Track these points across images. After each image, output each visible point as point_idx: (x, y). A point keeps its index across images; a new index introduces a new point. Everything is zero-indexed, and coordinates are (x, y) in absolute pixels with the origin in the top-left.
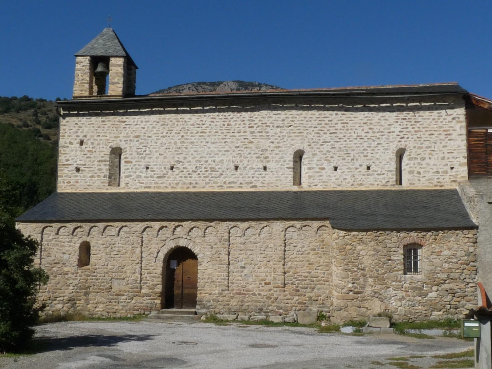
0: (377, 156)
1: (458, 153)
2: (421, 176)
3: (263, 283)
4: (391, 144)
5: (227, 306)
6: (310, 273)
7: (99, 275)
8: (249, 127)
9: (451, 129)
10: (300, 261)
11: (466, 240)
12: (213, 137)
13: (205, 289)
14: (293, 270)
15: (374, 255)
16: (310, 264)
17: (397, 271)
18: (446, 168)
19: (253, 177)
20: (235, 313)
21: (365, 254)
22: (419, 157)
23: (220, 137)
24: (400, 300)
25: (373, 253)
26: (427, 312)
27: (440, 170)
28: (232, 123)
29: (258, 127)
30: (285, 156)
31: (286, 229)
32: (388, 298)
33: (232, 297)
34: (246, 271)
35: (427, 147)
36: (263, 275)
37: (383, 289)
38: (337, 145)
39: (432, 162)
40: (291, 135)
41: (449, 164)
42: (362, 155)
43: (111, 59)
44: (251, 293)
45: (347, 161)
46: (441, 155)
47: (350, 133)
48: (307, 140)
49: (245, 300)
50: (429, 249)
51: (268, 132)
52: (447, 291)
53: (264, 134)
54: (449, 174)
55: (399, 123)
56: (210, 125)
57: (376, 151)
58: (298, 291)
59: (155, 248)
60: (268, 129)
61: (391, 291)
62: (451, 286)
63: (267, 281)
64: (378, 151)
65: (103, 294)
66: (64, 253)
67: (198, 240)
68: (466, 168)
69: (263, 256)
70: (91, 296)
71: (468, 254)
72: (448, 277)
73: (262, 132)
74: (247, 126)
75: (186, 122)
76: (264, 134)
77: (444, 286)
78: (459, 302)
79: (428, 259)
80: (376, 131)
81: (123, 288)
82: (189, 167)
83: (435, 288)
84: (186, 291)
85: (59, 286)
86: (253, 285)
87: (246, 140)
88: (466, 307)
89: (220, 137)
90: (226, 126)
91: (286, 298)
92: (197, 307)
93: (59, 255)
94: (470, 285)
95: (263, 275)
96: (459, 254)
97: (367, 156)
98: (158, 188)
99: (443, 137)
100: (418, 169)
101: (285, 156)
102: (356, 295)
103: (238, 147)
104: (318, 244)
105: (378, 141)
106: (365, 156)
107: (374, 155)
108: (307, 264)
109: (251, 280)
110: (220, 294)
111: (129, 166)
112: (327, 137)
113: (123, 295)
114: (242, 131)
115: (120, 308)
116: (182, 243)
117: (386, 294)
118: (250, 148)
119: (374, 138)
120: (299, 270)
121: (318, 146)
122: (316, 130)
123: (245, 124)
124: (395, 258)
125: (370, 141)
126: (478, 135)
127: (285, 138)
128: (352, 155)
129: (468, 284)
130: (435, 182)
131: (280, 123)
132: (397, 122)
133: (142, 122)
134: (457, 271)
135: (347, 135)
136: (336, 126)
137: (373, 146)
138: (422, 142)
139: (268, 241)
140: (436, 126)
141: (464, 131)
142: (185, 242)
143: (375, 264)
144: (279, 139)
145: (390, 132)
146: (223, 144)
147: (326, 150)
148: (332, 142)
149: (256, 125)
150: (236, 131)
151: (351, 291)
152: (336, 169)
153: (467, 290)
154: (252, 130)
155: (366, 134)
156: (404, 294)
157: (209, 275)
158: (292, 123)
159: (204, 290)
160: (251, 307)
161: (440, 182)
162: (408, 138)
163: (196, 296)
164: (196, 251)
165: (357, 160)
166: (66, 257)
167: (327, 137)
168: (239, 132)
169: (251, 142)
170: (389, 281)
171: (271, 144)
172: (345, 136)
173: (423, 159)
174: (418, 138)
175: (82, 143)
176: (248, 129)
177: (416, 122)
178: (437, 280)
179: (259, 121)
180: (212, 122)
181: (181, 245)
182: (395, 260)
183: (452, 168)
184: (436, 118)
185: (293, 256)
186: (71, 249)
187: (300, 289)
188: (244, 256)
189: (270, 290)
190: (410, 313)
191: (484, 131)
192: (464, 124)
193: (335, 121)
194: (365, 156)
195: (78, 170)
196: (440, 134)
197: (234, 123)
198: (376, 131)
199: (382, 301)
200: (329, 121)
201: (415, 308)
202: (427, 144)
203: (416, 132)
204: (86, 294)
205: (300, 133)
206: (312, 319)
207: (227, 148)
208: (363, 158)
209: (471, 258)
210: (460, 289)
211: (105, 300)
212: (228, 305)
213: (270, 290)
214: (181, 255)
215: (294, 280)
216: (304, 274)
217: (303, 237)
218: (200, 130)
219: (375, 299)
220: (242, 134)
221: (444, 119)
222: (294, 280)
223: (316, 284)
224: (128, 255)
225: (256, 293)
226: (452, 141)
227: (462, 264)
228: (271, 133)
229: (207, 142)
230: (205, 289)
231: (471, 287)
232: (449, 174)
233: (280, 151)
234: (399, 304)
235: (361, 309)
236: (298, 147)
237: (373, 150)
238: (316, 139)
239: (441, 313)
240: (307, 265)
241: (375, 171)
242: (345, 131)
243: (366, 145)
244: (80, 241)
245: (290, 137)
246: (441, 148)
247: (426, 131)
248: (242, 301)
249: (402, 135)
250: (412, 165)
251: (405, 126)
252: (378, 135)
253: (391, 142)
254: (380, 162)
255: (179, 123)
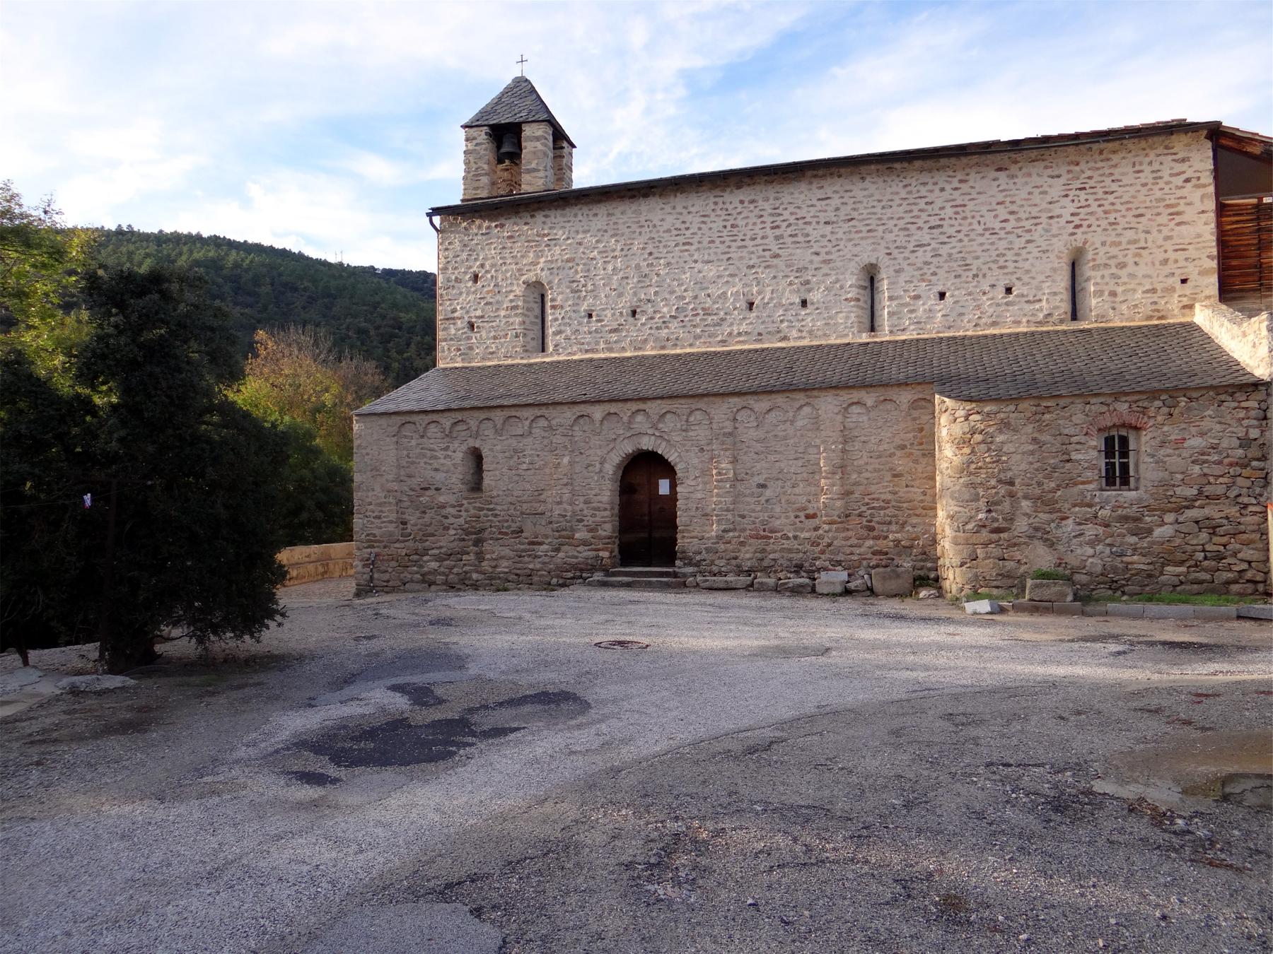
0: (1027, 265)
1: (1197, 249)
2: (1119, 299)
3: (802, 514)
4: (1055, 240)
5: (734, 562)
6: (895, 493)
7: (499, 507)
8: (772, 228)
9: (1182, 202)
10: (875, 470)
11: (1242, 414)
12: (706, 252)
13: (691, 528)
14: (861, 488)
15: (1032, 453)
16: (895, 476)
17: (1083, 483)
18: (1171, 281)
19: (782, 321)
20: (748, 573)
21: (1013, 450)
22: (1112, 262)
23: (719, 251)
24: (1092, 544)
25: (1031, 447)
26: (1151, 567)
27: (1159, 287)
28: (740, 222)
29: (789, 225)
30: (841, 277)
31: (846, 409)
32: (1065, 540)
33: (742, 544)
34: (768, 493)
35: (1129, 243)
36: (803, 499)
37: (1053, 521)
38: (944, 250)
39: (1141, 270)
40: (852, 236)
41: (1178, 272)
42: (994, 266)
43: (525, 127)
44: (779, 535)
45: (964, 279)
46: (1162, 256)
47: (970, 224)
48: (883, 244)
49: (768, 549)
50: (1155, 434)
51: (807, 235)
52: (1197, 522)
53: (800, 239)
54: (1179, 292)
55: (1070, 198)
56: (700, 229)
57: (1024, 256)
58: (872, 529)
59: (596, 455)
60: (809, 229)
61: (1069, 525)
62: (1207, 511)
63: (810, 512)
64: (1029, 256)
65: (506, 542)
66: (436, 470)
67: (676, 437)
68: (1214, 279)
69: (800, 463)
70: (487, 546)
71: (1245, 443)
72: (1200, 492)
73: (796, 235)
74: (768, 225)
75: (655, 226)
76: (800, 239)
77: (1191, 513)
78: (1225, 546)
79: (1153, 456)
80: (1023, 216)
81: (542, 530)
82: (665, 310)
83: (1170, 518)
84: (657, 535)
85: (430, 530)
86: (783, 520)
87: (767, 253)
88: (1240, 556)
89: (719, 251)
90: (729, 228)
91: (849, 543)
92: (678, 563)
93: (429, 473)
94: (1251, 508)
95: (803, 499)
96: (1225, 444)
97: (1005, 267)
98: (611, 350)
99: (1164, 219)
100: (1112, 287)
101: (841, 277)
102: (995, 536)
103: (753, 267)
104: (911, 435)
105: (1028, 237)
106: (1001, 268)
107: (1020, 265)
108: (888, 477)
109: (778, 510)
110: (719, 538)
111: (559, 314)
112: (925, 237)
113: (540, 544)
114: (759, 237)
115: (538, 566)
116: (647, 444)
117: (1060, 531)
118: (776, 266)
119: (1019, 231)
120: (873, 488)
121: (906, 255)
122: (901, 223)
123: (763, 222)
124: (1080, 457)
125: (1011, 237)
126: (1239, 210)
127: (842, 243)
128: (974, 267)
129: (1246, 506)
130: (1146, 309)
131: (830, 216)
132: (1067, 196)
133: (577, 232)
134: (1221, 480)
135: (965, 229)
136: (942, 212)
137: (1016, 246)
138: (1119, 231)
139: (810, 434)
140: (1148, 199)
141: (1211, 205)
142: (652, 443)
143: (1037, 470)
144: (830, 245)
145: (1051, 217)
146: (725, 263)
147: (921, 260)
148: (934, 245)
149: (785, 224)
150: (748, 237)
151: (984, 526)
152: (942, 295)
153: (1242, 520)
154: (777, 232)
155: (1004, 225)
156: (1101, 530)
157: (702, 503)
158: (855, 214)
159: (689, 531)
160: (779, 562)
161: (1158, 311)
162: (1089, 226)
163: (674, 541)
164: (672, 457)
165: (984, 276)
166: (440, 476)
167: (925, 237)
168: (754, 239)
169: (777, 256)
170: (1066, 506)
171: (815, 258)
172: (959, 231)
173: (1122, 266)
174: (1111, 224)
175: (476, 278)
176: (769, 232)
177: (1106, 193)
178: (1173, 500)
179: (792, 214)
180: (704, 222)
181: (645, 448)
182: (1077, 461)
183: (1184, 281)
184: (1150, 181)
185: (861, 462)
186: (448, 462)
187: (877, 526)
188: (763, 464)
189: (816, 529)
190: (1115, 570)
191: (1254, 201)
192: (1211, 189)
193: (939, 203)
194: (1001, 268)
195: (472, 326)
196: (1158, 214)
197: (744, 223)
198: (1023, 216)
199: (1052, 545)
200: (927, 203)
201: (1125, 559)
202: (1130, 234)
203: (1106, 212)
204: (478, 542)
205: (869, 231)
206: (905, 582)
207: (732, 269)
208: (997, 272)
209: (1254, 452)
210: (1227, 518)
211: (512, 554)
212: (735, 558)
213: (816, 529)
214: (644, 468)
215: (864, 508)
216: (883, 497)
217: (879, 424)
218: (681, 239)
219: (1036, 542)
220: (759, 241)
221: (1167, 183)
222: (864, 508)
223: (909, 516)
224: (547, 471)
225: (790, 535)
226: (1183, 227)
227: (1231, 465)
228: (814, 235)
229: (696, 262)
230: (691, 528)
231: (1255, 513)
232: (1179, 292)
233: (832, 269)
234: (1090, 551)
235: (1007, 563)
236: (867, 258)
237: (1017, 255)
238: (901, 240)
239: (1183, 569)
240: (890, 478)
241: (1023, 296)
242: (959, 221)
243: (1002, 245)
244: (464, 447)
245: (850, 240)
246: (1160, 242)
247: (1128, 209)
248: (764, 551)
249: (1077, 221)
250: (1099, 280)
251: (1083, 203)
252: (1027, 224)
253: (1054, 236)
254: (1033, 278)
255: (643, 230)
